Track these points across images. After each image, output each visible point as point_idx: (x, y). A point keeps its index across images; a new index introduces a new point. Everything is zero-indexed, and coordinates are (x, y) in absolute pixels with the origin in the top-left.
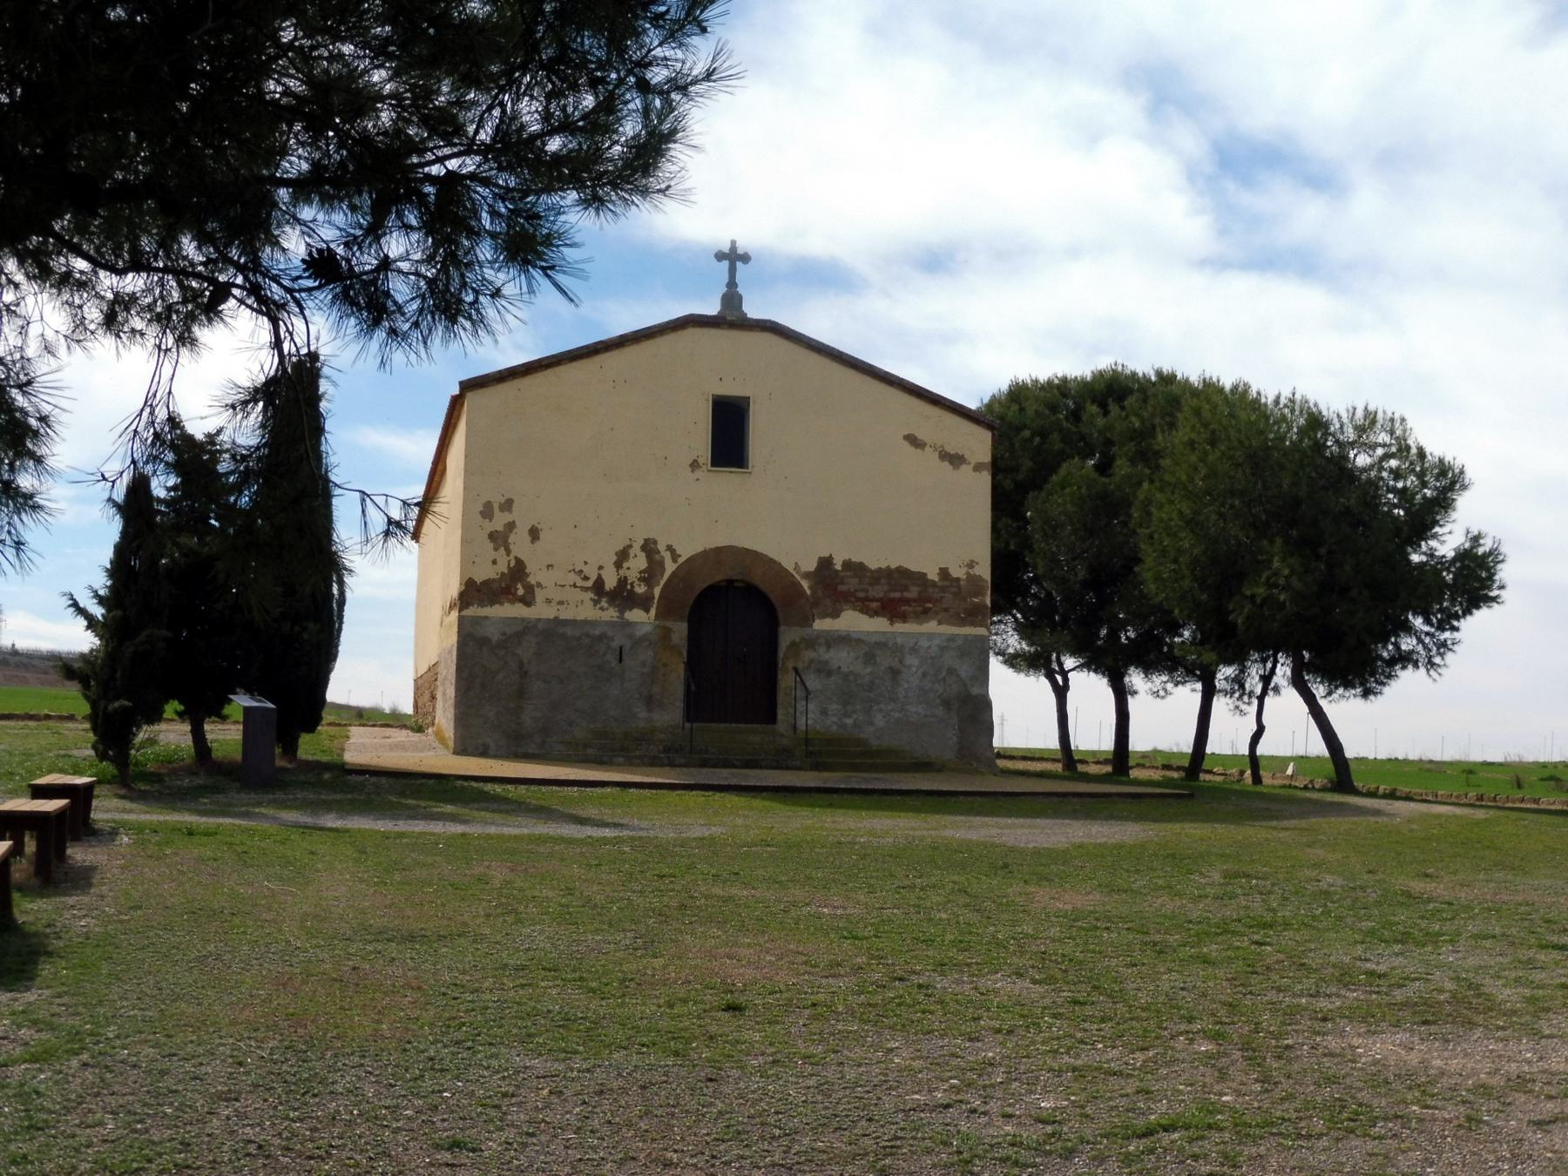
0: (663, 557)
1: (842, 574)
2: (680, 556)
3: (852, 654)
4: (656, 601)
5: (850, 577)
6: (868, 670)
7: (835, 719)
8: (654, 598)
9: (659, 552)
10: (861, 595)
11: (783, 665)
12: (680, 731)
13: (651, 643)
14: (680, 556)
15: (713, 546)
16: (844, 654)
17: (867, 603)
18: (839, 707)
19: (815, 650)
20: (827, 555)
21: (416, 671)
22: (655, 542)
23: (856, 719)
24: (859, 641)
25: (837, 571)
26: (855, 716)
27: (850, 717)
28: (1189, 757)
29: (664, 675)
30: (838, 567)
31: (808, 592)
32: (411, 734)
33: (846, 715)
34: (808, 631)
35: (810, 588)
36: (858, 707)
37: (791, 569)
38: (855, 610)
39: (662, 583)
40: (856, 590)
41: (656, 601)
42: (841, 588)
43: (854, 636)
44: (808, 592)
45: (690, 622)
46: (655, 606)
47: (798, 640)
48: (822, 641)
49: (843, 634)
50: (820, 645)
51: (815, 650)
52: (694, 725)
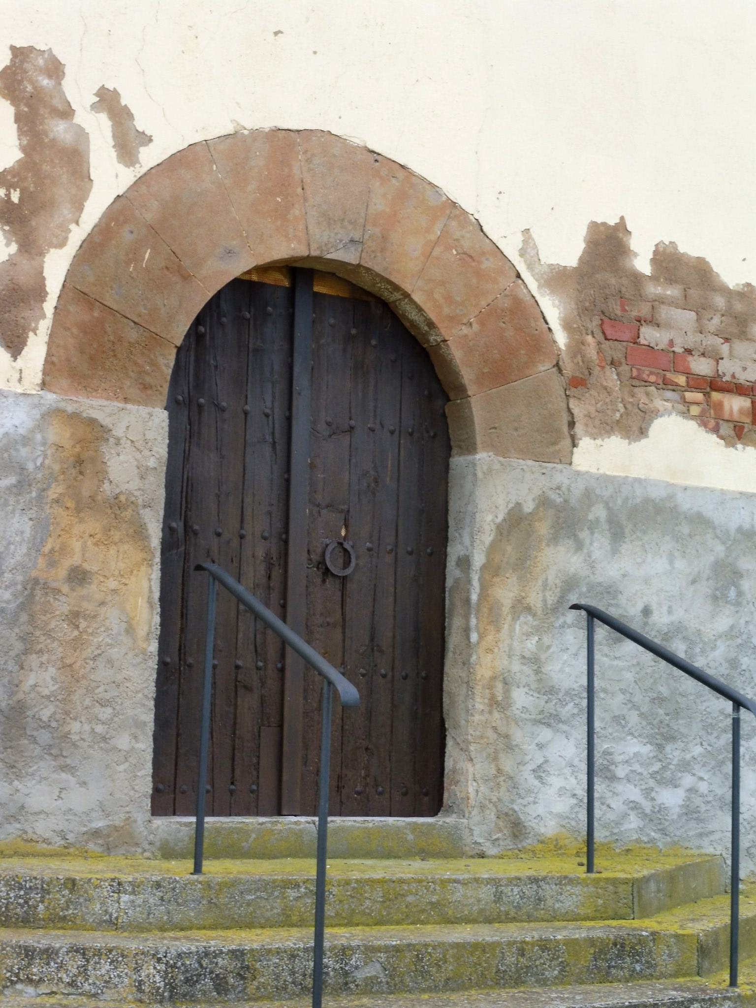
0: (82, 135)
1: (653, 290)
2: (147, 140)
3: (680, 564)
4: (49, 306)
5: (673, 303)
6: (723, 623)
7: (633, 793)
8: (40, 293)
9: (67, 113)
10: (702, 367)
11: (483, 595)
12: (573, 868)
13: (22, 486)
14: (147, 140)
15: (267, 124)
16: (657, 565)
17: (715, 396)
18: (646, 750)
19: (579, 546)
20: (612, 221)
21: (620, 641)
22: (55, 69)
23: (692, 790)
24: (700, 521)
25: (637, 278)
26: (688, 780)
27: (674, 784)
28: (328, 855)
29: (74, 617)
30: (643, 264)
31: (561, 338)
32: (367, 929)
33: (664, 779)
34: (561, 476)
35: (567, 326)
36: (697, 750)
37: (511, 249)
38: (686, 414)
39: (77, 235)
40: (689, 351)
41: (49, 306)
42: (649, 335)
43: (686, 504)
44: (561, 338)
45: (174, 406)
46: (45, 326)
47: (529, 507)
48: (599, 512)
49: (657, 494)
50: (593, 526)
51: (579, 546)
52: (336, 822)
